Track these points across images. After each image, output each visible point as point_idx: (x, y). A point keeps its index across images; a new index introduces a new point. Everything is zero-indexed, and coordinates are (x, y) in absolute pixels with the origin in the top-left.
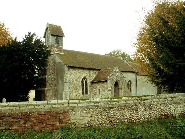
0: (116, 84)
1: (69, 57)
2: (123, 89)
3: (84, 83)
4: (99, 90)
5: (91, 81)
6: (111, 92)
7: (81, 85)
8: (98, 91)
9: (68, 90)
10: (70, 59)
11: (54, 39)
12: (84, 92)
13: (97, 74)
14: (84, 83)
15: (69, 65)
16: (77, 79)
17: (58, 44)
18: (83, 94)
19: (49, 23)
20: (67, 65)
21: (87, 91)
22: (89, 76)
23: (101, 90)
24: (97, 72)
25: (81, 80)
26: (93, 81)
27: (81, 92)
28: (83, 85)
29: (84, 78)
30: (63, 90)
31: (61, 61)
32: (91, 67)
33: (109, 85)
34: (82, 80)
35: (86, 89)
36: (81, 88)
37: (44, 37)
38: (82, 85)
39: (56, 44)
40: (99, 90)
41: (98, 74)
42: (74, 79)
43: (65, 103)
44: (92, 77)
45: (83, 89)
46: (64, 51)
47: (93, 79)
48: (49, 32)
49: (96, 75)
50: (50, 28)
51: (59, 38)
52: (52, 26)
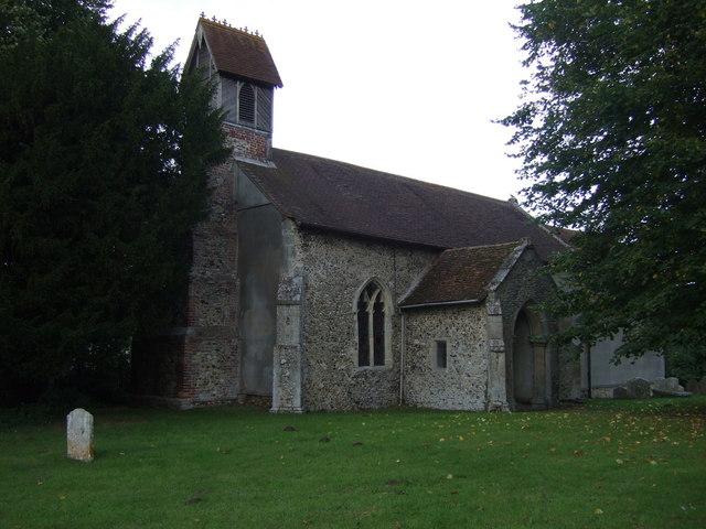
3: (370, 310)
14: (370, 310)
17: (251, 119)
34: (362, 296)
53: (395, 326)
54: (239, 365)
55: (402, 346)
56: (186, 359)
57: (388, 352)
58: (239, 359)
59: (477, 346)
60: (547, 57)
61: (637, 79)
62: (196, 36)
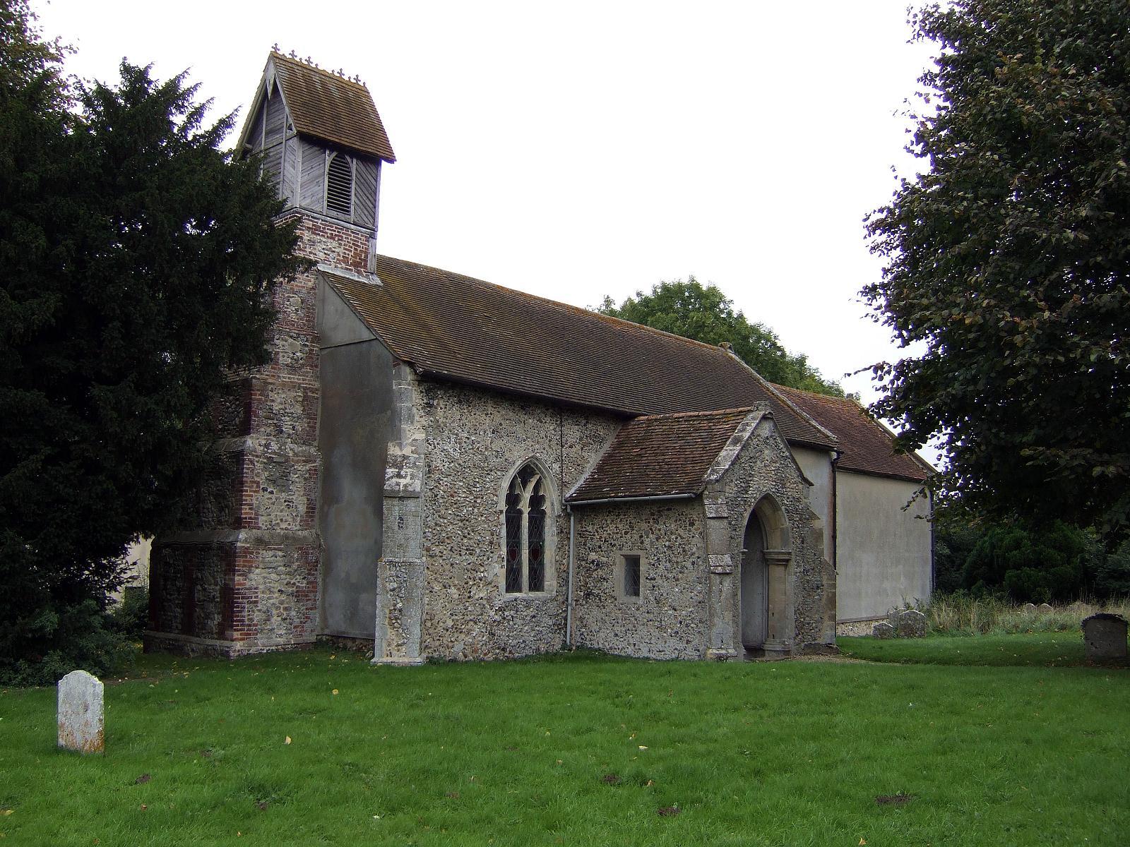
0: (757, 526)
1: (739, 360)
2: (793, 564)
3: (524, 506)
4: (633, 563)
5: (571, 491)
6: (727, 583)
7: (503, 518)
8: (619, 572)
9: (414, 554)
10: (425, 327)
11: (316, 172)
13: (606, 447)
14: (524, 506)
16: (476, 472)
17: (346, 210)
18: (513, 585)
19: (285, 51)
20: (411, 365)
21: (541, 564)
22: (560, 459)
23: (643, 568)
24: (609, 437)
25: (506, 484)
26: (581, 493)
27: (498, 571)
29: (526, 473)
30: (377, 552)
31: (366, 335)
32: (575, 395)
33: (718, 531)
34: (512, 486)
35: (537, 552)
36: (504, 542)
40: (633, 563)
41: (619, 446)
42: (460, 471)
44: (580, 467)
45: (513, 552)
46: (388, 266)
47: (581, 482)
48: (286, 115)
49: (601, 454)
50: (293, 87)
51: (354, 165)
54: (320, 588)
58: (319, 580)
59: (689, 564)
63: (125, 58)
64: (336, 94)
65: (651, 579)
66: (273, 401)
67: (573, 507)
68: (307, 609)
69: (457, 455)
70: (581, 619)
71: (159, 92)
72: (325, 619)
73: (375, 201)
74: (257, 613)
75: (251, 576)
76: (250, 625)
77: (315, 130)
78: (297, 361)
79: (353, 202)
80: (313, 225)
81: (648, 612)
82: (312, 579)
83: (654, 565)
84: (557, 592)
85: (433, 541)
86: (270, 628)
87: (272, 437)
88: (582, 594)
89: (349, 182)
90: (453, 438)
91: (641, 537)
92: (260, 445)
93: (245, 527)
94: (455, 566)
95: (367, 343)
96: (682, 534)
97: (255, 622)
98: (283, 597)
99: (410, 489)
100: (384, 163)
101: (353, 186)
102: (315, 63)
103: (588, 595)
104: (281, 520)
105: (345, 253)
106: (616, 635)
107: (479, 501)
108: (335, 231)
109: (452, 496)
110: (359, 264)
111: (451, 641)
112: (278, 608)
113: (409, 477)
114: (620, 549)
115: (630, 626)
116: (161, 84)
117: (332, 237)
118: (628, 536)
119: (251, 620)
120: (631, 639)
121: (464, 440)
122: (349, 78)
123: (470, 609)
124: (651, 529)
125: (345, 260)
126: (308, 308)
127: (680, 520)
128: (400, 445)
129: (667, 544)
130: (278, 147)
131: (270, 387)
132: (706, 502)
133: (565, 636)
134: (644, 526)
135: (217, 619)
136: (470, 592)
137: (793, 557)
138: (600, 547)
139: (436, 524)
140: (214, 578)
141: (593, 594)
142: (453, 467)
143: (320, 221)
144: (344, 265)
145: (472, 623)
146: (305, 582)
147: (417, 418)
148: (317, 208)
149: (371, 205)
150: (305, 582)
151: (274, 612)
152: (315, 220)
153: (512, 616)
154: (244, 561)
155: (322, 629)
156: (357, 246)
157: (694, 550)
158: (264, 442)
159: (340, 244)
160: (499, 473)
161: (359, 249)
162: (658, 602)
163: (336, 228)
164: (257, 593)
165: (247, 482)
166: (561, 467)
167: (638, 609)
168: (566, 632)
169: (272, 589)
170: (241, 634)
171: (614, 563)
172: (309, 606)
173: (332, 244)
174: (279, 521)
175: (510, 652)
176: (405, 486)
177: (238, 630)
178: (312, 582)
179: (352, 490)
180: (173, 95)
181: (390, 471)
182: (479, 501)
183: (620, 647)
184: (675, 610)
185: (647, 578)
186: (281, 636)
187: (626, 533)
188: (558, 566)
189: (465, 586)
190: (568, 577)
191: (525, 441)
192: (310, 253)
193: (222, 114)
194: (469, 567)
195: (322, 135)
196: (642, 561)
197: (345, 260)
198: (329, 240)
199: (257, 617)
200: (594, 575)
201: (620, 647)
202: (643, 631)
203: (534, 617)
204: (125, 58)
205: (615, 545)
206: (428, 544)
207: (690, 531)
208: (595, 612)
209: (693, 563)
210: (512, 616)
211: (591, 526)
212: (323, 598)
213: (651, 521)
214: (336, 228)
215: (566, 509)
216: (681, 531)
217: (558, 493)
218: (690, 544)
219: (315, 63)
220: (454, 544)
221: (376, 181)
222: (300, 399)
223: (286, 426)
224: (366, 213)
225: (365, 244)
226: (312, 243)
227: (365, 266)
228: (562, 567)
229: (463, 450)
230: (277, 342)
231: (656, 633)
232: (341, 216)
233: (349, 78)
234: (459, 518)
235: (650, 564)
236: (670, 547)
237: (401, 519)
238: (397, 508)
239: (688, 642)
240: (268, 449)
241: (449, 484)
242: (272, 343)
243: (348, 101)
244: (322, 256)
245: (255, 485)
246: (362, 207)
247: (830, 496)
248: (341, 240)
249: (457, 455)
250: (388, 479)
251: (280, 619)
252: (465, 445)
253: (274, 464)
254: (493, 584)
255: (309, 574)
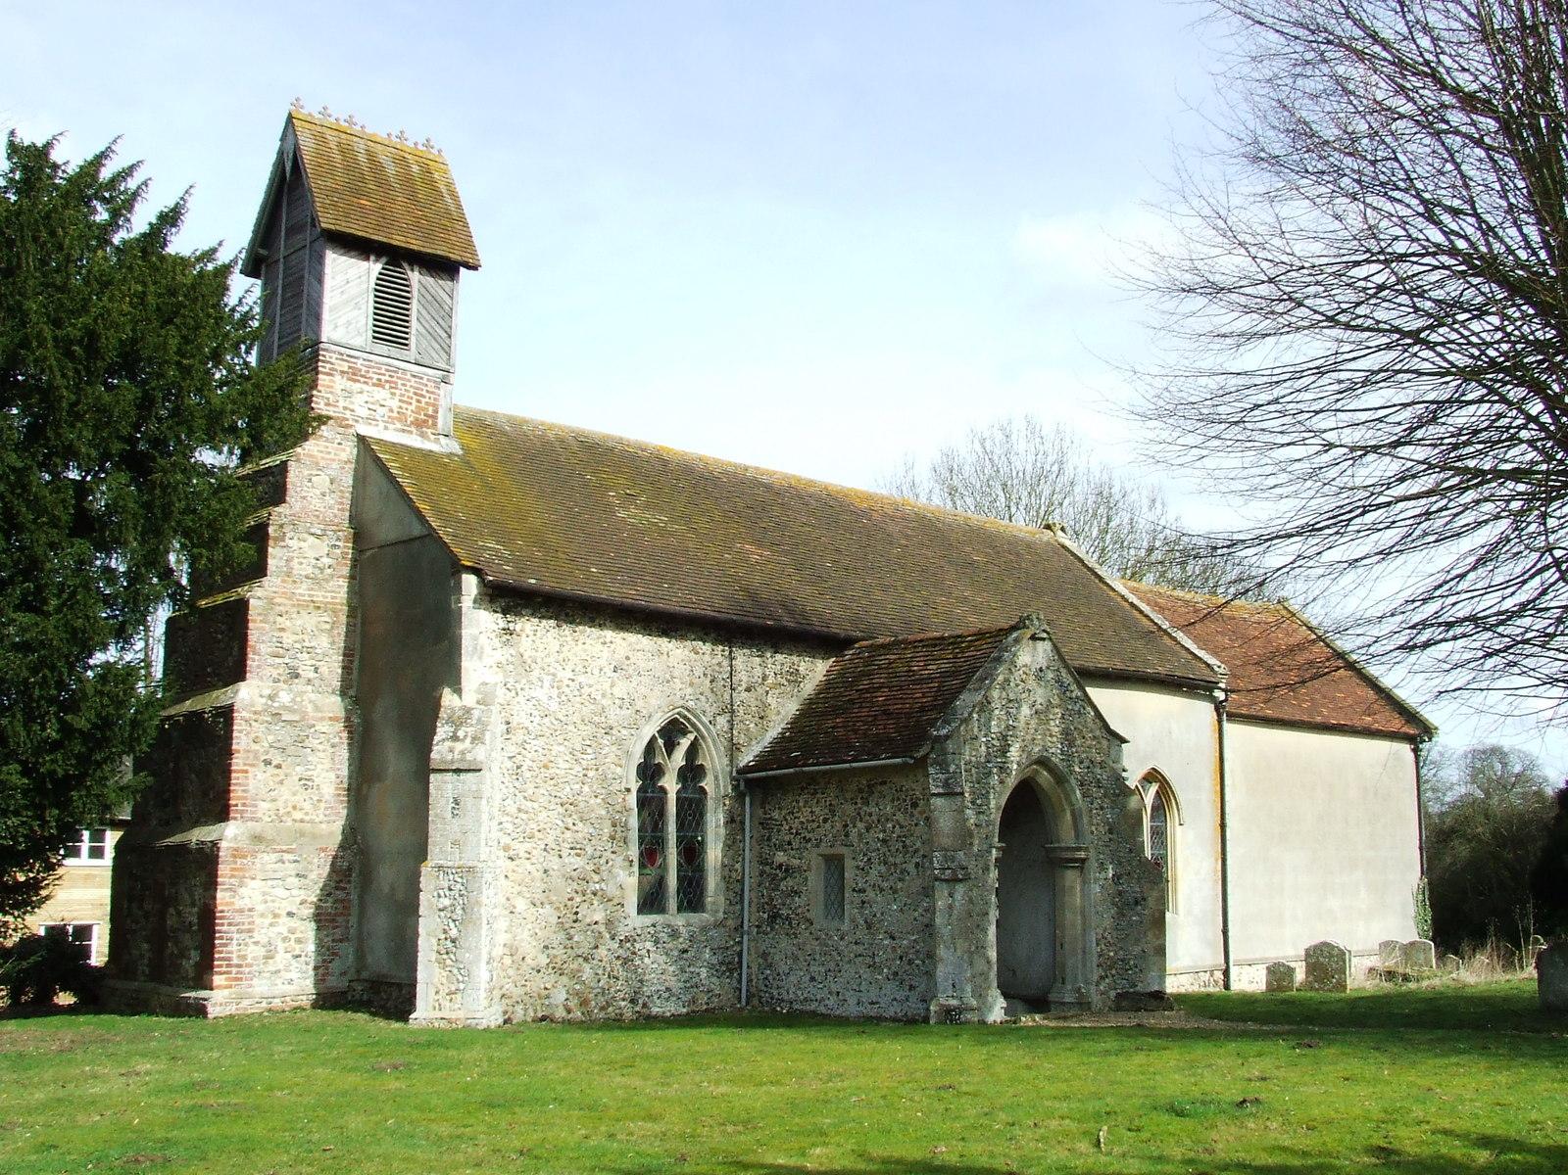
3: (671, 784)
5: (746, 758)
7: (632, 800)
8: (815, 881)
12: (680, 827)
14: (671, 784)
15: (506, 572)
17: (401, 342)
28: (650, 800)
29: (672, 731)
34: (650, 748)
35: (692, 852)
37: (254, 266)
38: (642, 803)
39: (378, 337)
43: (1553, 480)
51: (415, 277)
52: (345, 150)
53: (733, 821)
54: (355, 911)
55: (749, 871)
56: (221, 896)
57: (712, 882)
58: (354, 897)
59: (911, 868)
60: (372, 258)
61: (138, 767)
62: (281, 153)
63: (12, 133)
64: (391, 170)
65: (860, 891)
66: (282, 630)
67: (748, 782)
68: (333, 941)
69: (554, 706)
70: (765, 955)
71: (69, 180)
72: (360, 955)
73: (450, 327)
74: (252, 947)
75: (242, 891)
76: (240, 966)
77: (351, 225)
78: (321, 570)
79: (413, 331)
80: (350, 367)
81: (856, 943)
82: (340, 895)
83: (863, 869)
84: (725, 913)
85: (514, 835)
86: (274, 969)
87: (281, 684)
88: (766, 916)
89: (406, 301)
90: (547, 679)
91: (846, 826)
92: (261, 696)
93: (235, 819)
94: (551, 872)
95: (418, 542)
96: (901, 820)
97: (249, 961)
98: (294, 923)
99: (469, 757)
100: (462, 270)
101: (415, 306)
102: (437, 147)
103: (774, 917)
104: (294, 808)
105: (401, 407)
106: (813, 979)
107: (591, 774)
108: (398, 378)
109: (546, 767)
110: (424, 423)
111: (546, 989)
112: (285, 939)
113: (469, 740)
114: (817, 846)
115: (832, 966)
116: (72, 169)
117: (379, 384)
118: (828, 825)
119: (244, 957)
120: (833, 986)
121: (567, 682)
122: (416, 144)
123: (576, 938)
124: (859, 814)
125: (402, 417)
126: (341, 491)
127: (898, 799)
128: (458, 691)
129: (881, 836)
130: (300, 253)
131: (278, 609)
132: (931, 770)
133: (740, 981)
134: (850, 809)
135: (195, 956)
136: (576, 913)
137: (1092, 853)
138: (789, 843)
139: (519, 810)
140: (192, 895)
141: (780, 916)
142: (548, 724)
143: (360, 361)
144: (399, 425)
145: (581, 960)
146: (330, 900)
147: (488, 650)
148: (358, 342)
149: (444, 335)
150: (330, 900)
151: (281, 946)
152: (353, 360)
153: (648, 951)
154: (233, 869)
155: (358, 972)
156: (422, 396)
157: (918, 844)
158: (266, 692)
159: (393, 394)
160: (624, 732)
161: (423, 400)
162: (869, 927)
163: (387, 370)
164: (252, 917)
165: (238, 752)
166: (731, 722)
167: (842, 939)
168: (740, 975)
169: (277, 911)
170: (226, 979)
171: (809, 869)
172: (337, 937)
173: (381, 394)
174: (290, 809)
175: (645, 1005)
176: (463, 753)
177: (221, 973)
178: (342, 901)
179: (394, 761)
180: (87, 183)
181: (442, 731)
182: (591, 774)
183: (818, 997)
184: (894, 939)
185: (854, 890)
186: (291, 982)
187: (825, 821)
188: (727, 873)
189: (569, 903)
190: (742, 890)
191: (668, 682)
192: (345, 408)
193: (166, 202)
194: (574, 874)
195: (360, 234)
196: (849, 863)
197: (402, 417)
198: (376, 388)
199: (254, 952)
200: (782, 886)
201: (818, 997)
202: (848, 971)
203: (685, 951)
204: (12, 133)
205: (810, 839)
206: (506, 840)
207: (912, 815)
208: (785, 944)
209: (917, 865)
210: (648, 951)
211: (777, 811)
212: (360, 924)
213: (859, 801)
214: (387, 370)
215: (739, 785)
216: (899, 816)
217: (726, 761)
218: (912, 835)
219: (437, 147)
220: (550, 840)
221: (451, 298)
222: (328, 626)
223: (305, 668)
224: (437, 346)
225: (432, 393)
226: (349, 394)
227: (435, 425)
228: (734, 875)
229: (563, 698)
230: (290, 543)
231: (865, 973)
232: (394, 351)
233: (416, 144)
234: (558, 800)
235: (858, 867)
236: (884, 841)
237: (456, 802)
238: (450, 786)
239: (911, 988)
240: (273, 701)
241: (540, 750)
242: (283, 544)
243: (407, 180)
244: (364, 412)
245: (251, 755)
246: (429, 337)
247: (1213, 760)
248: (396, 388)
249: (554, 706)
250: (437, 744)
251: (289, 955)
252: (567, 690)
253: (283, 724)
254: (616, 901)
255: (337, 888)
